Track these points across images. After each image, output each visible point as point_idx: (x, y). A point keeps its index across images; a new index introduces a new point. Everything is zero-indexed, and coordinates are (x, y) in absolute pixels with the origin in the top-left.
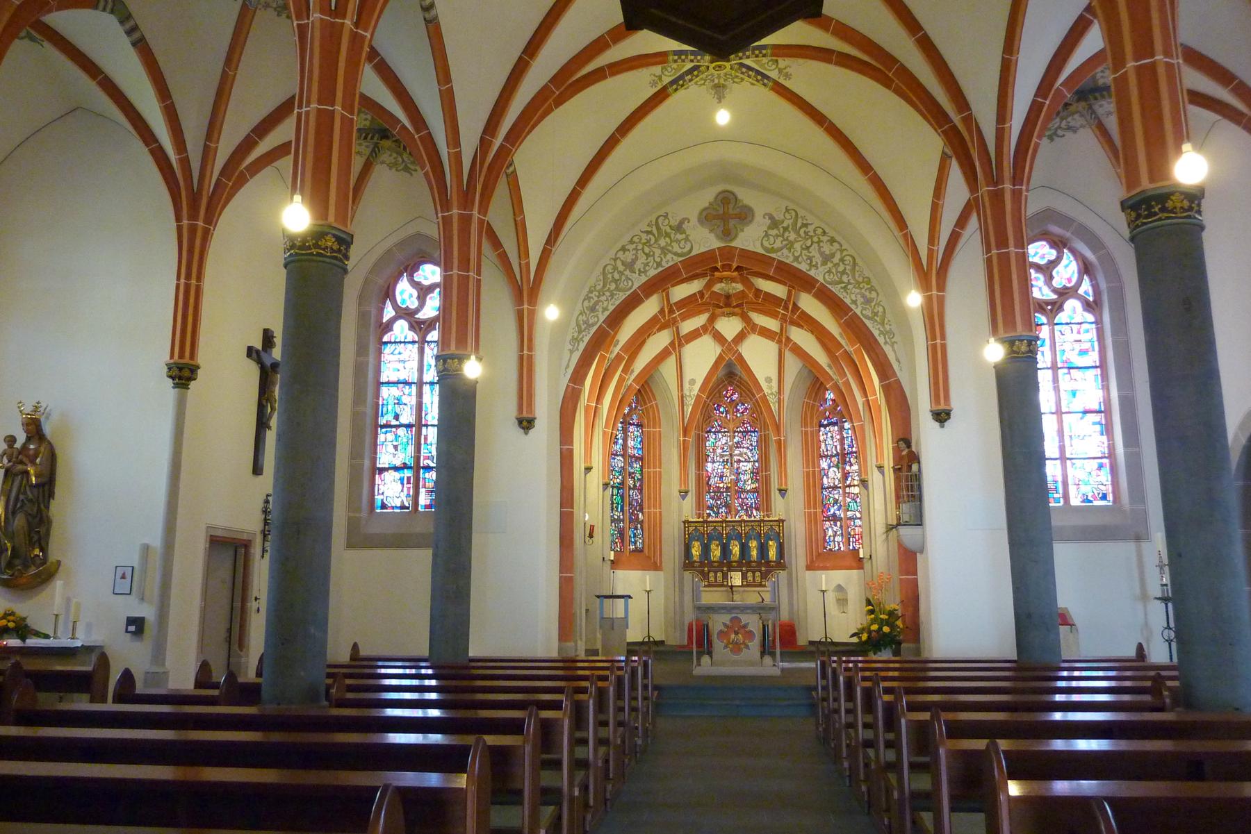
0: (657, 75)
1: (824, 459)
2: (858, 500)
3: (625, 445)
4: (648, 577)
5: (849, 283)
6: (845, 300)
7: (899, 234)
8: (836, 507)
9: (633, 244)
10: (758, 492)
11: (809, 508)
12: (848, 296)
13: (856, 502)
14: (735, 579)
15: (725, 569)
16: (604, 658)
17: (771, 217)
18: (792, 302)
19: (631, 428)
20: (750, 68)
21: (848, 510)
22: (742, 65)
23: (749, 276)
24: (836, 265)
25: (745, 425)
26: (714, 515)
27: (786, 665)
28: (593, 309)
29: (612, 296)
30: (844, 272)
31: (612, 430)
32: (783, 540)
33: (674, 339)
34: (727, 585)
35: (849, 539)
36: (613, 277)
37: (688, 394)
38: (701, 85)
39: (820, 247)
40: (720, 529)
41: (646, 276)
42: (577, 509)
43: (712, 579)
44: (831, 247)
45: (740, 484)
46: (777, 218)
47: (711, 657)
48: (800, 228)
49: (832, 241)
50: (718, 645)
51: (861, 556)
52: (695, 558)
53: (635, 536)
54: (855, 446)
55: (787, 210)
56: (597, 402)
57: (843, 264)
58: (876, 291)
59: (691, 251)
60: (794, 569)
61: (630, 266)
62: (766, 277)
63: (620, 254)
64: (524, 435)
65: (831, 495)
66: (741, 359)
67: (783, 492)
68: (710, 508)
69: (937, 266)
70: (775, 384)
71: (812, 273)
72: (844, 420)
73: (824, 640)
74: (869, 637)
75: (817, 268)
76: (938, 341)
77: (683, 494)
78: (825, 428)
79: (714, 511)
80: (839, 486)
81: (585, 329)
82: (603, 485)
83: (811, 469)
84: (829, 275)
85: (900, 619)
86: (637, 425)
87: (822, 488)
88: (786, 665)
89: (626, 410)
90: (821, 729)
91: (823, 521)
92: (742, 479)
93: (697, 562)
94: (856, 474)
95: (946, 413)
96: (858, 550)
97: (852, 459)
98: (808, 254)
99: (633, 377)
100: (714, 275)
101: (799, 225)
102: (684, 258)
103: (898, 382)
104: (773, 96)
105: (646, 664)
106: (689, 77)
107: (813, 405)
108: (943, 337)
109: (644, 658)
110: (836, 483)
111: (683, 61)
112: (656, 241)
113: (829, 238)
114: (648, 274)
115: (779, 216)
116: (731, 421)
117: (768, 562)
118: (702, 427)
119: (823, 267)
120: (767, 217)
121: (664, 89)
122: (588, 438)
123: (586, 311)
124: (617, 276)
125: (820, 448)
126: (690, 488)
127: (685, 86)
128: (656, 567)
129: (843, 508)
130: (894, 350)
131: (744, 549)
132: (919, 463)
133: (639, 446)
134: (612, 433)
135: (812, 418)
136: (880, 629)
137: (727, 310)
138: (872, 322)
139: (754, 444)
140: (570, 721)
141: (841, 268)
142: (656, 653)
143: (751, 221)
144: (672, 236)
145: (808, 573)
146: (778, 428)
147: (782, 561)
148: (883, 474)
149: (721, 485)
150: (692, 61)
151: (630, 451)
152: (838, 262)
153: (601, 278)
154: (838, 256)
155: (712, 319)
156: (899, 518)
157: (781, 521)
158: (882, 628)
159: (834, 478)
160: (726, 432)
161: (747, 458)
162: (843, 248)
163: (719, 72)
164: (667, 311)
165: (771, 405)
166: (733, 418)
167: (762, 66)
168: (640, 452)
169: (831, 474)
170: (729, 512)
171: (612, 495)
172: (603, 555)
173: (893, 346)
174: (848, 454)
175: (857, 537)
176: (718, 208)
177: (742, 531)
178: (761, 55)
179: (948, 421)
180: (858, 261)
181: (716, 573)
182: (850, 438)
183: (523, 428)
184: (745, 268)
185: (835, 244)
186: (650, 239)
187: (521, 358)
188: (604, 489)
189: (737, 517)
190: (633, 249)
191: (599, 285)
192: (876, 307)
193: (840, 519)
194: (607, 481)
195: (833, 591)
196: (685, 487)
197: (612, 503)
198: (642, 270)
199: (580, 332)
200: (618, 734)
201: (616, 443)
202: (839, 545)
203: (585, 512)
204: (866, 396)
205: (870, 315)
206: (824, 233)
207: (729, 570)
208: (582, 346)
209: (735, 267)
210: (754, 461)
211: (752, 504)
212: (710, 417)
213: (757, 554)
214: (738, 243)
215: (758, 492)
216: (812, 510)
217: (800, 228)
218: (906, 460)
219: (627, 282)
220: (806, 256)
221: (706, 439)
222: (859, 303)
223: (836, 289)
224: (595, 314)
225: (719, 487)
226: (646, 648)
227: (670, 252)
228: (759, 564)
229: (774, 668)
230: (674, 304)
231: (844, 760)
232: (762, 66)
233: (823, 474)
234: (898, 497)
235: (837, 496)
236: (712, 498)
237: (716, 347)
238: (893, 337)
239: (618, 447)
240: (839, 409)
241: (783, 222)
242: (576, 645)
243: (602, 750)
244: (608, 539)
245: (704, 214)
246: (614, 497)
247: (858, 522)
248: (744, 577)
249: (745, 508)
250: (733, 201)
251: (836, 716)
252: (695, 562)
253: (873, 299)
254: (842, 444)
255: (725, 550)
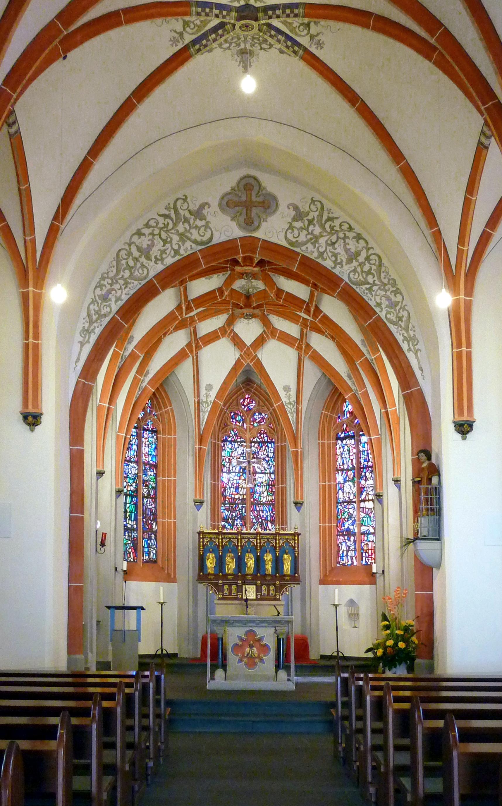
0: (178, 31)
1: (340, 473)
2: (372, 516)
3: (139, 451)
4: (161, 588)
5: (374, 284)
6: (369, 302)
7: (428, 232)
8: (350, 522)
9: (149, 228)
10: (273, 505)
11: (324, 522)
12: (373, 298)
13: (370, 517)
14: (249, 592)
15: (240, 582)
16: (116, 673)
17: (296, 208)
18: (314, 304)
19: (146, 434)
20: (279, 31)
21: (362, 525)
22: (270, 26)
23: (270, 273)
24: (361, 265)
25: (262, 436)
26: (229, 527)
27: (300, 679)
28: (105, 298)
29: (126, 284)
30: (369, 272)
31: (126, 435)
32: (298, 554)
33: (191, 340)
34: (241, 599)
35: (362, 553)
36: (127, 263)
37: (204, 400)
38: (226, 49)
39: (345, 244)
40: (235, 541)
41: (162, 263)
42: (88, 515)
43: (226, 592)
44: (357, 245)
45: (256, 496)
46: (302, 210)
47: (225, 671)
48: (326, 222)
49: (359, 237)
50: (232, 658)
51: (374, 570)
52: (210, 571)
53: (149, 546)
54: (371, 460)
55: (313, 201)
56: (110, 403)
57: (369, 263)
58: (401, 294)
59: (211, 239)
60: (307, 584)
61: (146, 253)
62: (290, 275)
63: (135, 239)
64: (30, 432)
65: (346, 510)
66: (259, 364)
67: (298, 505)
68: (225, 520)
69: (465, 270)
70: (293, 392)
71: (337, 271)
72: (361, 433)
73: (335, 654)
74: (384, 653)
75: (342, 266)
76: (464, 348)
77: (199, 503)
78: (342, 442)
79: (229, 523)
80: (354, 500)
81: (97, 319)
82: (116, 491)
83: (327, 483)
84: (354, 275)
85: (415, 636)
86: (152, 431)
87: (338, 503)
88: (300, 679)
89: (141, 415)
90: (340, 749)
91: (337, 535)
92: (258, 491)
93: (211, 574)
94: (371, 488)
95: (468, 424)
96: (371, 565)
97: (367, 474)
98: (334, 251)
99: (147, 380)
100: (234, 270)
101: (325, 218)
102: (203, 247)
103: (420, 392)
104: (302, 65)
105: (158, 678)
106: (214, 36)
107: (331, 417)
108: (469, 345)
109: (156, 673)
110: (351, 498)
111: (207, 15)
112: (175, 225)
113: (355, 235)
114: (165, 263)
115: (304, 207)
116: (248, 430)
117: (283, 576)
118: (218, 436)
119: (348, 265)
120: (291, 207)
121: (186, 48)
122: (100, 441)
123: (98, 299)
124: (131, 263)
125: (337, 461)
126: (205, 499)
127: (208, 48)
128: (170, 578)
129: (357, 522)
130: (417, 357)
131: (259, 561)
132: (439, 476)
133: (153, 453)
134: (125, 438)
135: (329, 432)
136: (396, 644)
137: (246, 311)
138: (396, 327)
139: (271, 455)
140: (66, 753)
141: (366, 268)
142: (169, 666)
143: (275, 211)
144: (192, 221)
145: (321, 587)
146: (295, 439)
147: (296, 575)
148: (399, 487)
149: (237, 497)
150: (217, 16)
151: (144, 458)
152: (363, 260)
153: (115, 263)
154: (364, 254)
155: (230, 322)
156: (416, 533)
157: (297, 534)
158: (397, 644)
159: (349, 493)
160: (242, 442)
161: (263, 469)
162: (369, 246)
163: (246, 33)
164: (184, 308)
165: (289, 415)
166: (250, 427)
167: (293, 30)
168: (154, 460)
169: (347, 489)
170: (244, 525)
171: (126, 503)
172: (115, 564)
173: (416, 354)
174: (363, 468)
175: (370, 552)
176: (240, 194)
177: (257, 543)
178: (292, 15)
179: (470, 434)
180: (385, 261)
181: (230, 585)
182: (366, 452)
183: (29, 424)
184: (268, 262)
185: (361, 241)
186: (168, 223)
187: (26, 347)
188: (117, 497)
189: (252, 529)
190: (150, 234)
191: (112, 271)
192: (401, 311)
193: (354, 534)
194: (120, 487)
195: (345, 606)
196: (200, 497)
197: (126, 512)
198: (158, 257)
199: (91, 322)
200: (127, 760)
201: (130, 449)
202: (352, 559)
203: (97, 519)
204: (386, 408)
205: (395, 320)
206: (350, 229)
207: (244, 583)
208: (93, 338)
209: (256, 262)
210: (270, 473)
211: (267, 516)
212: (226, 425)
213: (272, 567)
214: (259, 234)
215: (273, 505)
216: (327, 525)
217: (326, 222)
218: (426, 473)
219: (143, 270)
220: (330, 252)
221: (222, 448)
222: (383, 306)
223: (360, 290)
224: (107, 304)
225: (234, 498)
226: (158, 661)
227: (189, 239)
228: (273, 577)
229: (289, 682)
230: (191, 300)
231: (369, 785)
232: (293, 30)
233: (338, 488)
234: (416, 511)
235: (351, 511)
236: (227, 510)
237: (236, 353)
238: (416, 345)
239: (132, 454)
240: (356, 421)
241: (307, 214)
242: (86, 657)
243: (108, 780)
244: (121, 549)
245: (226, 199)
246: (128, 505)
247: (371, 537)
248: (258, 590)
249: (260, 520)
250: (256, 188)
251: (360, 736)
252: (210, 574)
253: (399, 302)
254: (358, 458)
255: (240, 563)
